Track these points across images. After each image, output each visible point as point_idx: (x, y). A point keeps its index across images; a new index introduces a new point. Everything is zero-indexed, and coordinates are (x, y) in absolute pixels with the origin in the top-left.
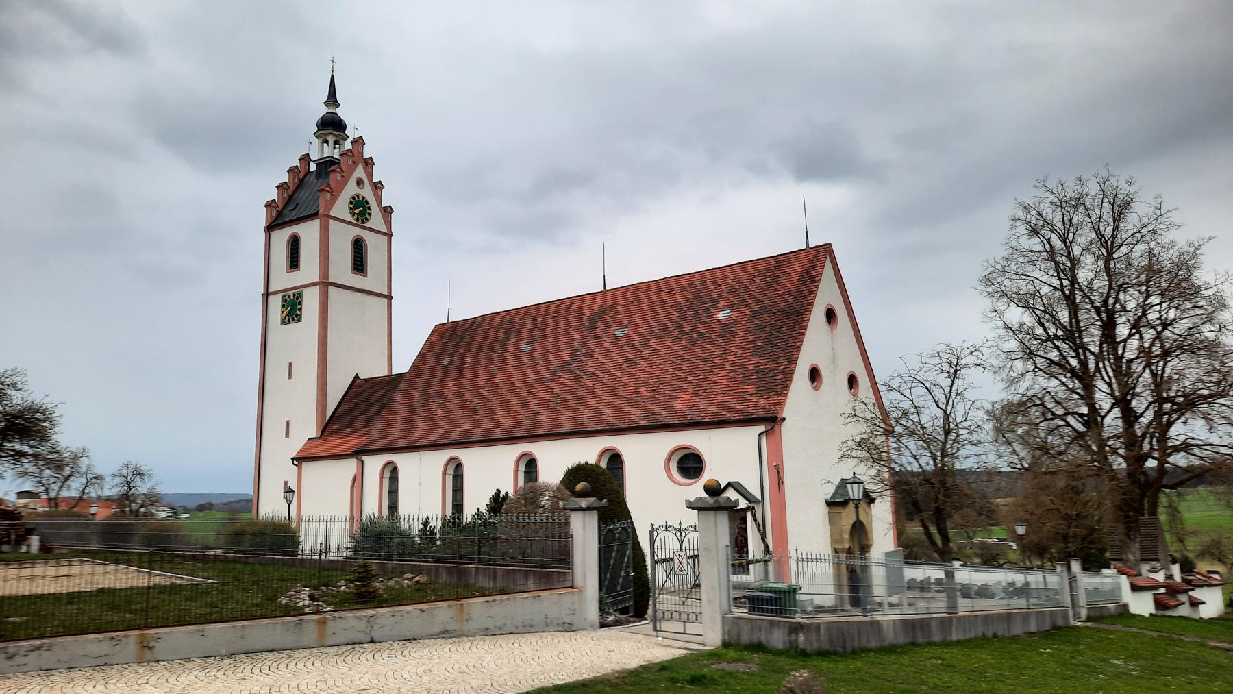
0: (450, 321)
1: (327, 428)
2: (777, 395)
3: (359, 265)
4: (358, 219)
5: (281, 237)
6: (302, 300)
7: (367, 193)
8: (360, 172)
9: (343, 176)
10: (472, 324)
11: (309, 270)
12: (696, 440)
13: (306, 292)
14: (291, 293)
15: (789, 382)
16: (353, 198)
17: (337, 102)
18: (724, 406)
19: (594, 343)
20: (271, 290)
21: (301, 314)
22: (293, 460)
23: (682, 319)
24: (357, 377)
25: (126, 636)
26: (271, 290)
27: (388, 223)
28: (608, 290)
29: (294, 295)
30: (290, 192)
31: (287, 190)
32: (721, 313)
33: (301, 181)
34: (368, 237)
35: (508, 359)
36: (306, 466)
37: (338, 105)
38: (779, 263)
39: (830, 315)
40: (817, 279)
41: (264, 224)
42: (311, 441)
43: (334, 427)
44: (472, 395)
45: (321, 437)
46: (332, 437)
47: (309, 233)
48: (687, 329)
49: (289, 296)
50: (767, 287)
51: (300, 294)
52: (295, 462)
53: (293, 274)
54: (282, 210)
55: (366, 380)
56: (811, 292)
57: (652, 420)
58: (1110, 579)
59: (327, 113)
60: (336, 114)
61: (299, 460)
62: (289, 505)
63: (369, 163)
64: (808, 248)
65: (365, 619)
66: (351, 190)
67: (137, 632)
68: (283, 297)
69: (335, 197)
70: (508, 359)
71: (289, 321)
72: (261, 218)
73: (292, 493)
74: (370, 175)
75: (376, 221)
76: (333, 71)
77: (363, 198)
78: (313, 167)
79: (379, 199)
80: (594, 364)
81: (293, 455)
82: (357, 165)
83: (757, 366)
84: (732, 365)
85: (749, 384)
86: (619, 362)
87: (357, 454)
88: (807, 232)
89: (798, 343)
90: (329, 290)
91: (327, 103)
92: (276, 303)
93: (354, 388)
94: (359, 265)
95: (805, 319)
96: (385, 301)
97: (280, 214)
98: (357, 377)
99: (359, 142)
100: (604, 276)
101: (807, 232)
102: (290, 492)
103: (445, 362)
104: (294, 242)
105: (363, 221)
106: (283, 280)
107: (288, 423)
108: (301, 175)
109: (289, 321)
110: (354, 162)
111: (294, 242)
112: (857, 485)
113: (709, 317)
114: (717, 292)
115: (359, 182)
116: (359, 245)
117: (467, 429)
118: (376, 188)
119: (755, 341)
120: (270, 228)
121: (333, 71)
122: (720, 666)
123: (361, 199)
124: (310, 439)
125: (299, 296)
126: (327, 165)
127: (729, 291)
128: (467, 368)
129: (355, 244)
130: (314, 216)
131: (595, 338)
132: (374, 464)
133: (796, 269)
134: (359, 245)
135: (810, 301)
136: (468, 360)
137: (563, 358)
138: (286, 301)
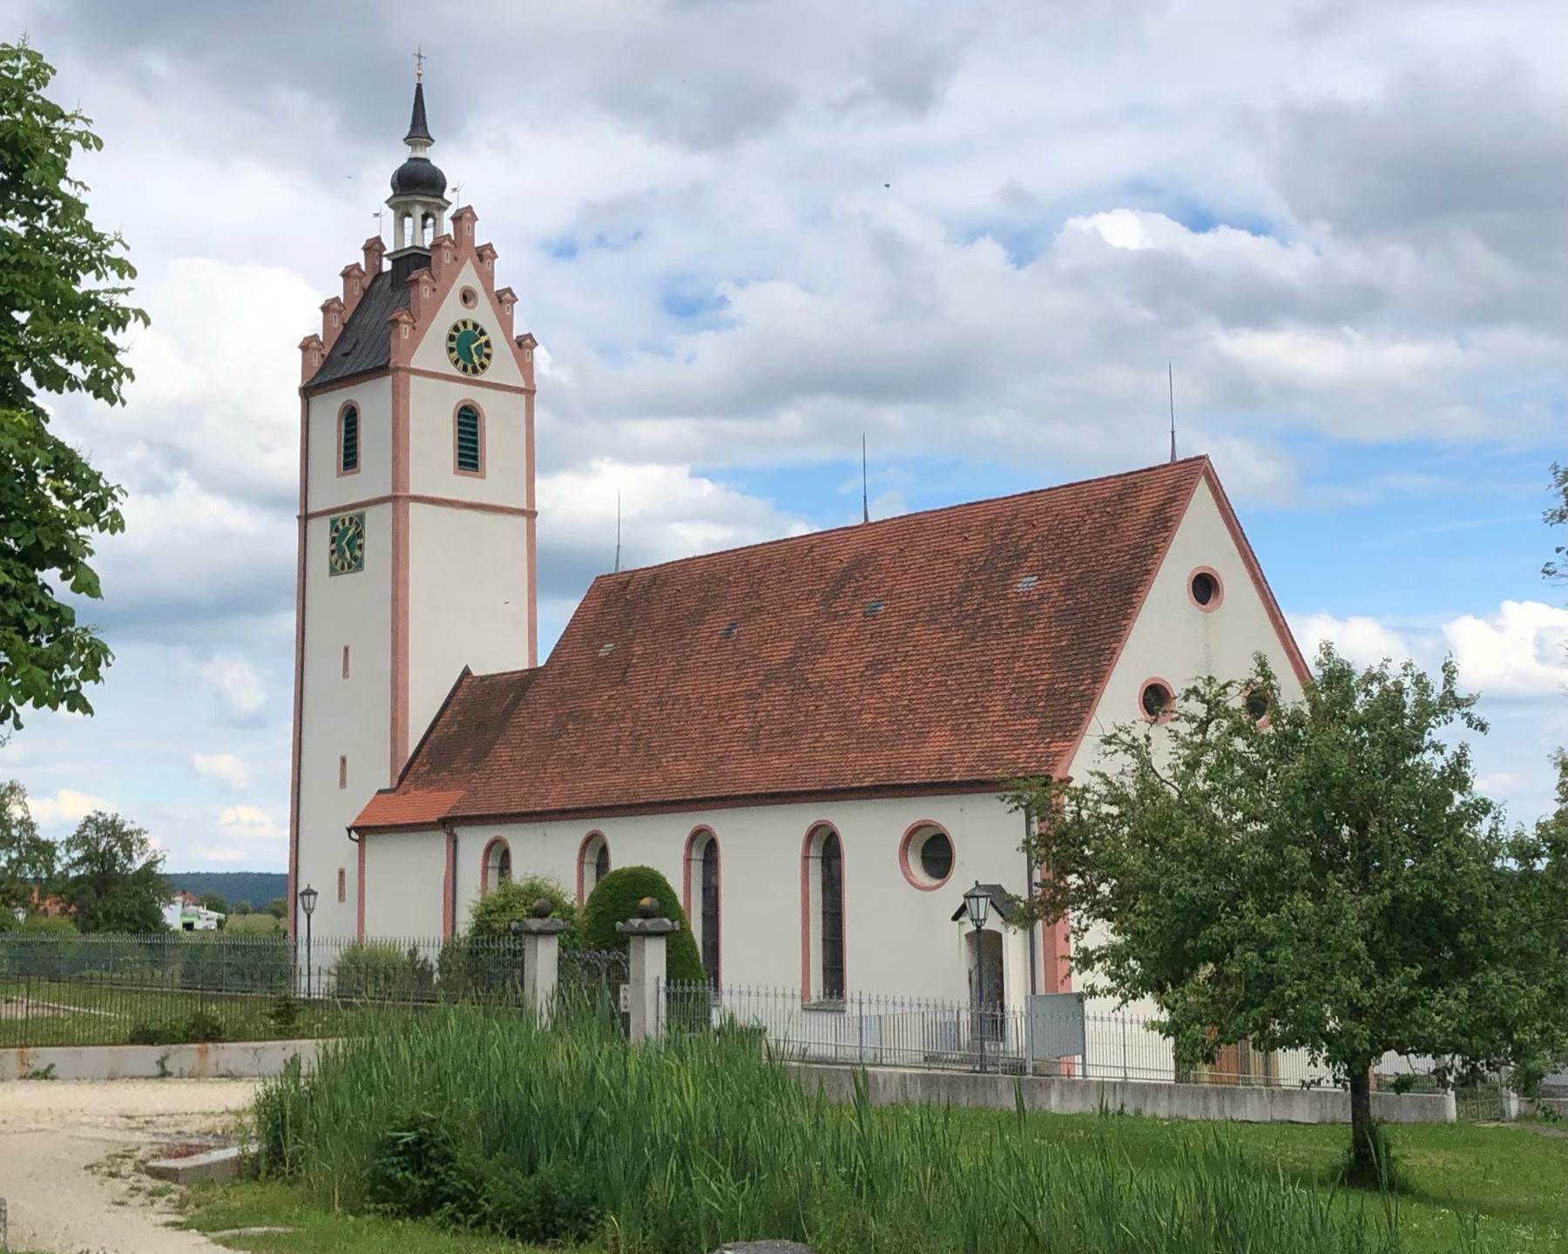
0: (620, 570)
1: (409, 774)
2: (1065, 738)
3: (469, 456)
4: (465, 369)
5: (330, 406)
6: (363, 527)
7: (483, 313)
8: (468, 276)
9: (434, 290)
10: (655, 577)
11: (372, 478)
12: (947, 814)
13: (371, 514)
14: (346, 515)
15: (1085, 715)
16: (456, 328)
17: (429, 137)
18: (985, 757)
19: (833, 627)
20: (311, 510)
21: (362, 556)
22: (349, 830)
23: (968, 587)
24: (466, 672)
25: (7, 1053)
26: (311, 510)
27: (527, 369)
28: (871, 524)
29: (351, 520)
30: (347, 315)
31: (340, 312)
32: (1025, 580)
33: (367, 292)
34: (486, 401)
35: (699, 652)
36: (378, 848)
37: (429, 141)
38: (1129, 486)
39: (1205, 587)
40: (1169, 524)
41: (297, 381)
42: (380, 796)
43: (423, 770)
44: (635, 719)
45: (398, 787)
46: (416, 789)
47: (372, 400)
48: (971, 609)
49: (343, 521)
50: (1100, 534)
51: (361, 517)
52: (355, 835)
53: (350, 479)
54: (352, 319)
55: (483, 679)
56: (1156, 550)
57: (883, 777)
58: (782, 1007)
59: (410, 160)
60: (427, 161)
61: (362, 832)
62: (309, 917)
63: (485, 255)
64: (1174, 463)
65: (252, 1052)
66: (450, 312)
67: (17, 1050)
68: (333, 522)
69: (418, 334)
70: (699, 652)
71: (342, 568)
72: (292, 374)
73: (312, 897)
74: (487, 279)
75: (502, 367)
76: (419, 75)
77: (475, 326)
78: (387, 266)
79: (506, 323)
80: (826, 665)
81: (350, 822)
82: (463, 264)
83: (1051, 683)
84: (1018, 680)
85: (1033, 715)
86: (861, 666)
87: (448, 824)
88: (1173, 433)
89: (1114, 645)
90: (411, 512)
91: (411, 139)
92: (321, 531)
93: (460, 694)
94: (469, 456)
95: (1134, 600)
96: (523, 520)
97: (328, 362)
98: (466, 672)
99: (464, 218)
100: (865, 498)
101: (1173, 433)
102: (309, 894)
103: (603, 653)
104: (350, 417)
105: (475, 371)
106: (335, 491)
107: (343, 760)
108: (367, 282)
109: (342, 568)
110: (456, 259)
111: (350, 417)
112: (975, 899)
113: (1005, 587)
114: (1028, 539)
115: (467, 297)
116: (468, 420)
117: (616, 784)
118: (500, 301)
119: (1058, 638)
120: (307, 392)
121: (419, 75)
122: (562, 1102)
123: (470, 328)
124: (380, 792)
125: (359, 522)
126: (412, 262)
127: (1046, 538)
128: (635, 666)
129: (459, 416)
130: (381, 370)
131: (835, 616)
132: (473, 843)
133: (1147, 501)
134: (468, 420)
135: (1149, 568)
136: (638, 650)
137: (778, 655)
138: (337, 530)
